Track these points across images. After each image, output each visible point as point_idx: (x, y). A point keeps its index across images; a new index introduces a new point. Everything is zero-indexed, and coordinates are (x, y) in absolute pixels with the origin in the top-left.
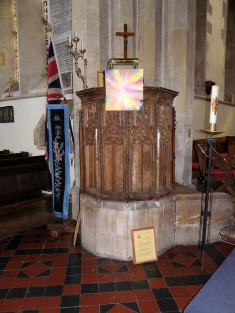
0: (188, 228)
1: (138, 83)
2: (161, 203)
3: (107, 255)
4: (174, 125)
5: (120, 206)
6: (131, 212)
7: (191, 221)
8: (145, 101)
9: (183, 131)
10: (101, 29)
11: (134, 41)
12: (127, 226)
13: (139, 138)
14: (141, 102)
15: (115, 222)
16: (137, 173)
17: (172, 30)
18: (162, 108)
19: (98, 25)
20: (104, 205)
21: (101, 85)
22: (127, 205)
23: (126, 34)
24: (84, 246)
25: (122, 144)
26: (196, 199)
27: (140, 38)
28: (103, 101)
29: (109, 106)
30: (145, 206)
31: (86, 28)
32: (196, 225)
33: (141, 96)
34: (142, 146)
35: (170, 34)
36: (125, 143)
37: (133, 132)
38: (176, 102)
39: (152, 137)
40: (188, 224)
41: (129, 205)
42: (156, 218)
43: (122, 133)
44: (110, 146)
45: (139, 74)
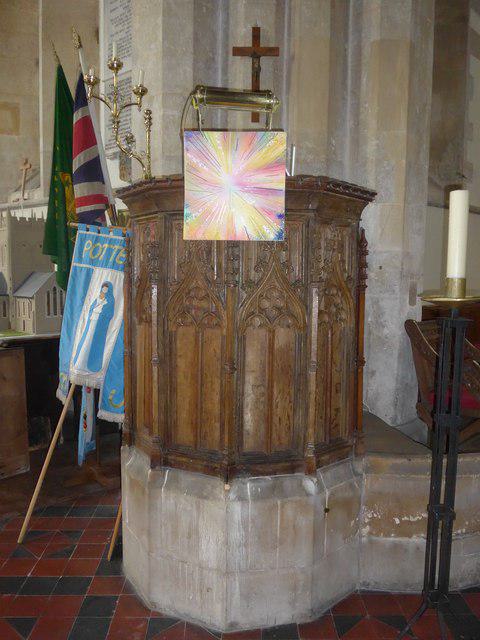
0: (396, 547)
1: (269, 168)
2: (319, 483)
3: (176, 611)
4: (362, 277)
5: (209, 487)
6: (237, 507)
7: (405, 530)
8: (289, 215)
9: (397, 289)
10: (196, 40)
11: (277, 69)
12: (226, 543)
13: (262, 310)
14: (279, 221)
15: (197, 533)
16: (257, 401)
17: (372, 40)
18: (329, 233)
19: (190, 29)
20: (173, 481)
21: (181, 172)
22: (227, 487)
23: (257, 51)
24: (128, 577)
25: (218, 325)
26: (415, 471)
27: (292, 58)
28: (178, 214)
29: (195, 227)
30: (275, 490)
31: (160, 38)
32: (419, 540)
33: (279, 203)
34: (272, 332)
35: (367, 51)
36: (225, 324)
37: (245, 295)
38: (371, 219)
39: (298, 310)
40: (398, 535)
41: (231, 486)
42: (305, 522)
43: (219, 298)
44: (192, 330)
45: (275, 145)
